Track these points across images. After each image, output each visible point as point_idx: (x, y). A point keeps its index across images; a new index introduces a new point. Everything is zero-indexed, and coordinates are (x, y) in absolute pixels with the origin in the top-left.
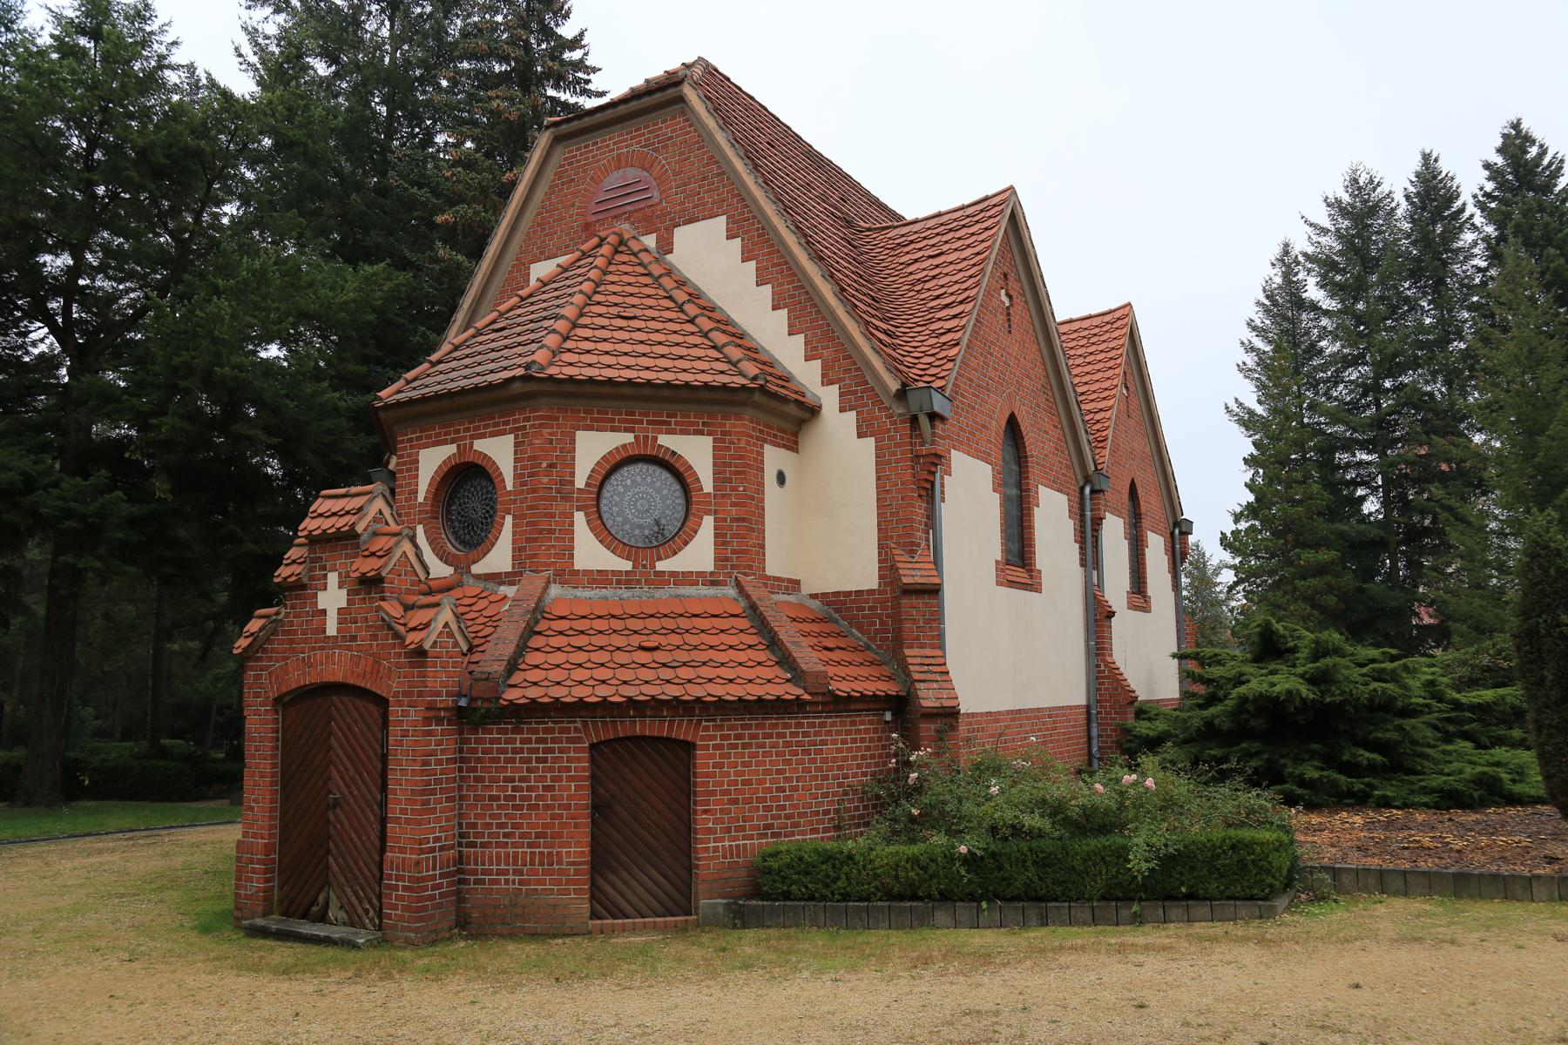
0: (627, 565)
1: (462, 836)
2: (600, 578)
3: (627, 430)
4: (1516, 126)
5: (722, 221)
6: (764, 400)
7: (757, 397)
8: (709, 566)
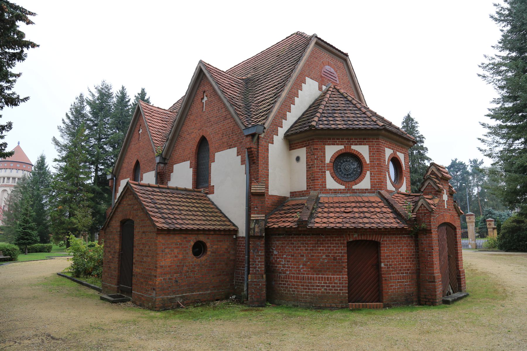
0: (343, 187)
1: (186, 250)
2: (335, 191)
3: (341, 145)
4: (409, 115)
5: (235, 150)
6: (387, 133)
7: (383, 132)
8: (369, 187)
